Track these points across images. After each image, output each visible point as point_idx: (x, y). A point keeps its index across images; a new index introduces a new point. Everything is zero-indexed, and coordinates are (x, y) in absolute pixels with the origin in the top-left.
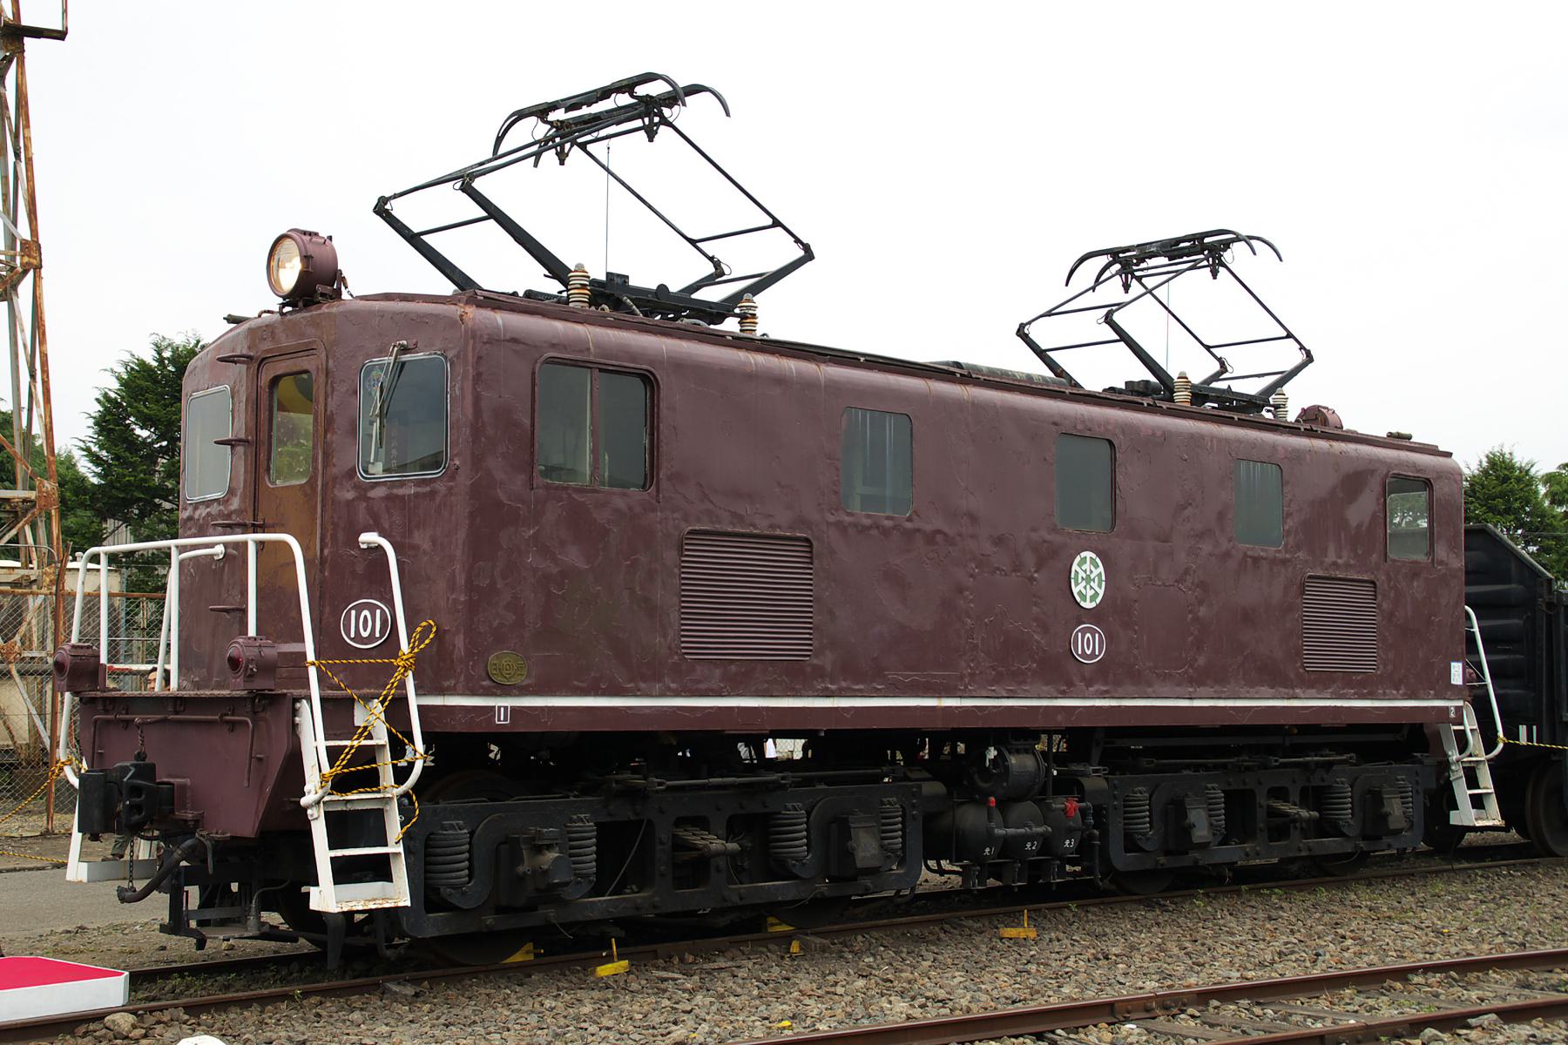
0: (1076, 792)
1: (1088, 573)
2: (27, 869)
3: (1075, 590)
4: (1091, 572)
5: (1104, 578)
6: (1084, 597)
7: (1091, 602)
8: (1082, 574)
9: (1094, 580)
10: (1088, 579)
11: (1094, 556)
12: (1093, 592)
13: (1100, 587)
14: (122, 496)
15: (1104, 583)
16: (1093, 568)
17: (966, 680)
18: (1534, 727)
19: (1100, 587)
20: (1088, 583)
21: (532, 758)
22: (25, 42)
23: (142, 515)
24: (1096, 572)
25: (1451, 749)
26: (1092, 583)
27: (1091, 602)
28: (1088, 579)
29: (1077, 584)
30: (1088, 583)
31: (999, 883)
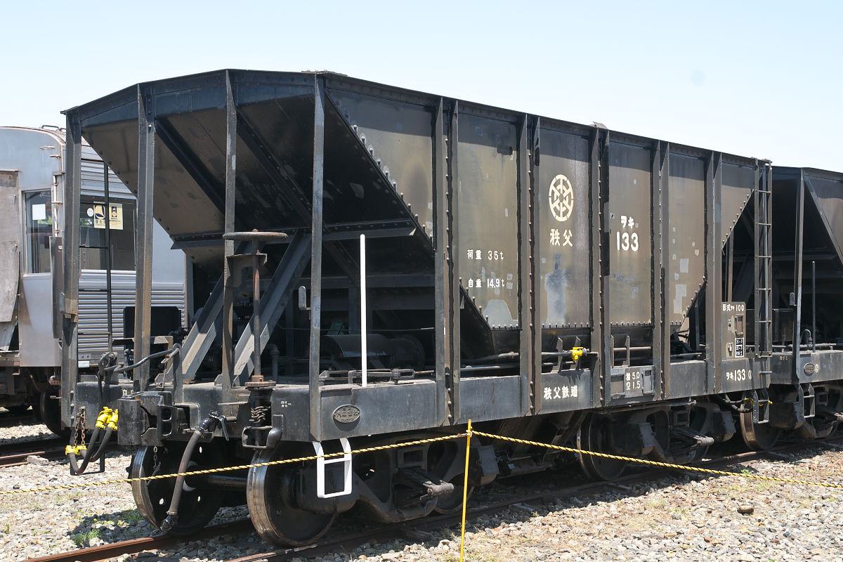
0: (579, 444)
1: (561, 192)
2: (591, 186)
3: (552, 206)
5: (550, 199)
6: (565, 183)
7: (559, 180)
9: (565, 198)
10: (562, 198)
12: (558, 188)
14: (301, 193)
15: (550, 195)
16: (565, 189)
20: (561, 201)
21: (31, 408)
23: (718, 430)
24: (556, 204)
26: (564, 201)
27: (559, 180)
28: (562, 198)
29: (569, 195)
30: (561, 195)
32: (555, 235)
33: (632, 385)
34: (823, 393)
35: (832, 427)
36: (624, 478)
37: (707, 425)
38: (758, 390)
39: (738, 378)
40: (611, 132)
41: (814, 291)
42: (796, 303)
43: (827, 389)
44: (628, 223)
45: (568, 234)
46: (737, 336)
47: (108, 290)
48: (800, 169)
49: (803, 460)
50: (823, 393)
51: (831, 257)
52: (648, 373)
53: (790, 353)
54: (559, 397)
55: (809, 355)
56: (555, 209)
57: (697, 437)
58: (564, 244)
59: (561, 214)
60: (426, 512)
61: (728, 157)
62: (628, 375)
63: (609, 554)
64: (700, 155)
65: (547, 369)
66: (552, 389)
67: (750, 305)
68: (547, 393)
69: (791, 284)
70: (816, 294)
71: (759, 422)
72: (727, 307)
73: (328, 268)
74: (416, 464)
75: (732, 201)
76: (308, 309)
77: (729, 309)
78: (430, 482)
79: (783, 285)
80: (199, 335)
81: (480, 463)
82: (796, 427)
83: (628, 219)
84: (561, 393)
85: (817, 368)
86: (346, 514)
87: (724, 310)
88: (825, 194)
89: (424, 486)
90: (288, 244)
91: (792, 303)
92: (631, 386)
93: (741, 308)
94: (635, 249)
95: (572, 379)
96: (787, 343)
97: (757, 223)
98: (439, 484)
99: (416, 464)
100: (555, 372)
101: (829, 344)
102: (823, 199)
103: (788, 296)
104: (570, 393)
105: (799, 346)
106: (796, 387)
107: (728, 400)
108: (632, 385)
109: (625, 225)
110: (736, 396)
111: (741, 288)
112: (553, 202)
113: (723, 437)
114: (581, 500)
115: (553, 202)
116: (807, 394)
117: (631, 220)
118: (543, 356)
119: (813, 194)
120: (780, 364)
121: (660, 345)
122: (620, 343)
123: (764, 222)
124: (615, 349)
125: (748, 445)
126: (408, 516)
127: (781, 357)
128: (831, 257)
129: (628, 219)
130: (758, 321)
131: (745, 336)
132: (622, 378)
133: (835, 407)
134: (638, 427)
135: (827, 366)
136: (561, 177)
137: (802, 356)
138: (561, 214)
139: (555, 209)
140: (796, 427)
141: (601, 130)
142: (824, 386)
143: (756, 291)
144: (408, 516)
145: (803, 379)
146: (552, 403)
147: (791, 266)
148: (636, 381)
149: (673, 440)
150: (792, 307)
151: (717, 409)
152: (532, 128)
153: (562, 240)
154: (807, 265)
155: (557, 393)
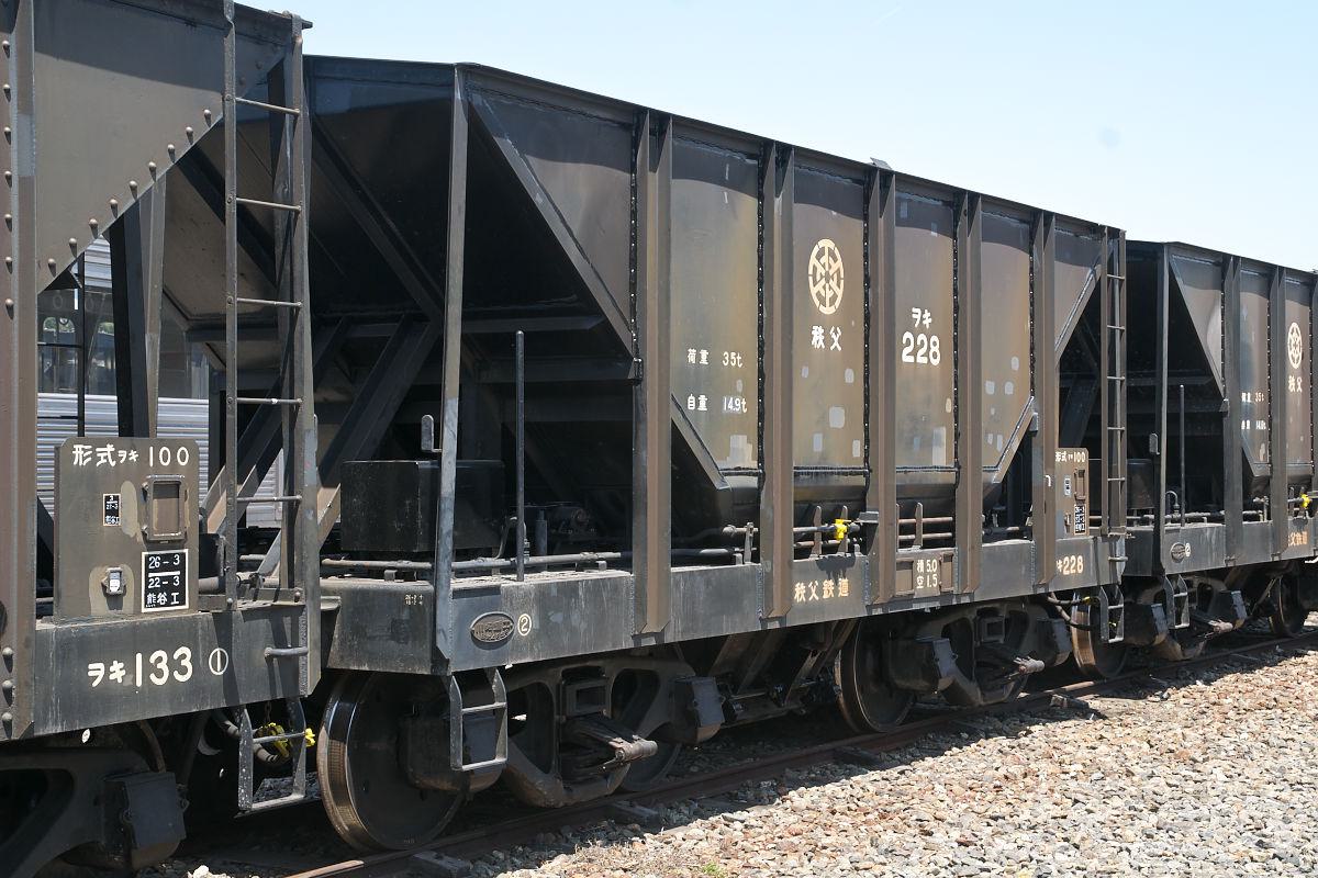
3: (814, 291)
4: (824, 287)
5: (811, 278)
6: (832, 254)
8: (820, 270)
9: (822, 277)
10: (828, 277)
11: (822, 308)
13: (814, 267)
15: (811, 272)
17: (990, 728)
18: (76, 308)
19: (815, 268)
20: (827, 273)
22: (896, 235)
23: (1046, 647)
24: (819, 287)
25: (451, 398)
28: (828, 277)
30: (827, 273)
31: (1228, 625)
32: (818, 334)
33: (925, 580)
34: (996, 620)
35: (1012, 684)
36: (445, 841)
37: (1029, 640)
38: (1105, 587)
39: (1071, 568)
40: (898, 174)
41: (1183, 431)
42: (1160, 450)
43: (1004, 614)
44: (922, 319)
45: (836, 332)
46: (152, 544)
47: (81, 418)
48: (448, 68)
49: (1310, 652)
50: (996, 620)
51: (1204, 381)
52: (949, 558)
53: (1150, 528)
54: (817, 598)
55: (495, 590)
56: (818, 294)
57: (1019, 661)
58: (832, 348)
59: (828, 303)
60: (610, 787)
61: (1065, 220)
62: (920, 565)
63: (939, 837)
64: (860, 176)
65: (802, 553)
66: (806, 585)
67: (1094, 453)
68: (800, 589)
69: (1151, 422)
70: (527, 424)
71: (1111, 641)
72: (1061, 456)
73: (1178, 415)
74: (593, 709)
75: (1072, 288)
76: (434, 451)
77: (1064, 459)
78: (620, 740)
79: (1140, 424)
80: (322, 490)
81: (696, 704)
82: (1156, 643)
83: (923, 313)
84: (820, 591)
85: (525, 624)
86: (481, 795)
87: (1058, 460)
88: (551, 150)
89: (612, 747)
90: (386, 339)
91: (427, 444)
92: (925, 584)
93: (1081, 457)
94: (936, 362)
95: (833, 569)
96: (1142, 512)
97: (1106, 326)
98: (631, 740)
99: (593, 709)
100: (813, 558)
101: (595, 556)
102: (550, 164)
103: (1146, 440)
104: (836, 591)
105: (1164, 516)
106: (445, 681)
107: (1053, 599)
108: (925, 580)
109: (918, 322)
110: (1065, 595)
111: (1081, 429)
112: (815, 284)
113: (1055, 659)
114: (1165, 679)
115: (815, 284)
116: (1177, 591)
117: (927, 314)
118: (795, 534)
119: (1179, 281)
120: (405, 615)
121: (971, 512)
122: (908, 512)
123: (1116, 324)
124: (795, 529)
125: (347, 838)
126: (581, 794)
127: (408, 597)
128: (588, 324)
129: (923, 313)
130: (1106, 480)
131: (1087, 500)
132: (910, 565)
133: (1018, 646)
134: (930, 644)
135: (567, 618)
136: (826, 244)
137: (458, 594)
138: (828, 303)
139: (818, 294)
140: (1156, 643)
141: (882, 171)
142: (997, 605)
143: (229, 406)
144: (581, 794)
145: (1170, 568)
146: (807, 607)
147: (1152, 394)
148: (931, 574)
149: (566, 746)
150: (428, 455)
151: (1044, 617)
152: (885, 186)
153: (828, 341)
154: (1173, 390)
155: (813, 591)
